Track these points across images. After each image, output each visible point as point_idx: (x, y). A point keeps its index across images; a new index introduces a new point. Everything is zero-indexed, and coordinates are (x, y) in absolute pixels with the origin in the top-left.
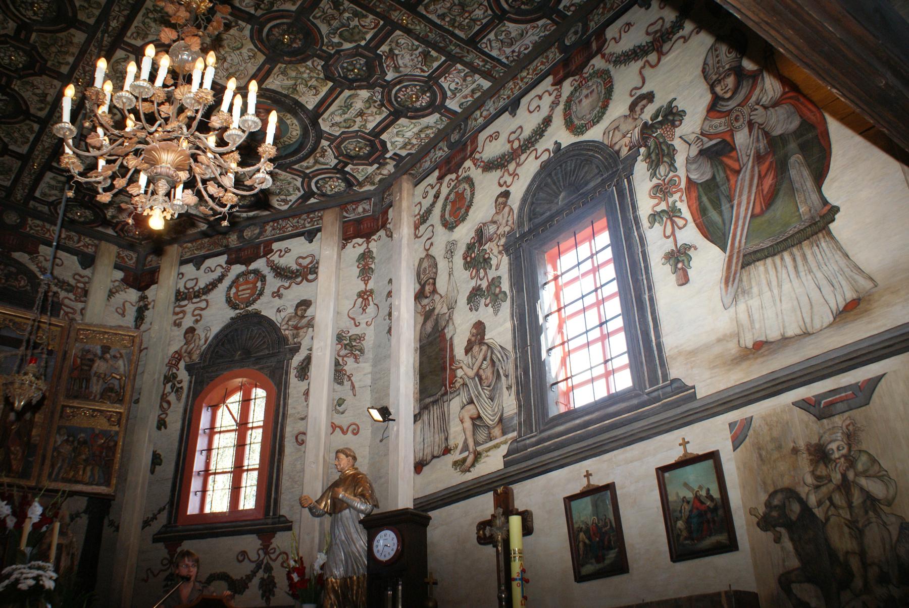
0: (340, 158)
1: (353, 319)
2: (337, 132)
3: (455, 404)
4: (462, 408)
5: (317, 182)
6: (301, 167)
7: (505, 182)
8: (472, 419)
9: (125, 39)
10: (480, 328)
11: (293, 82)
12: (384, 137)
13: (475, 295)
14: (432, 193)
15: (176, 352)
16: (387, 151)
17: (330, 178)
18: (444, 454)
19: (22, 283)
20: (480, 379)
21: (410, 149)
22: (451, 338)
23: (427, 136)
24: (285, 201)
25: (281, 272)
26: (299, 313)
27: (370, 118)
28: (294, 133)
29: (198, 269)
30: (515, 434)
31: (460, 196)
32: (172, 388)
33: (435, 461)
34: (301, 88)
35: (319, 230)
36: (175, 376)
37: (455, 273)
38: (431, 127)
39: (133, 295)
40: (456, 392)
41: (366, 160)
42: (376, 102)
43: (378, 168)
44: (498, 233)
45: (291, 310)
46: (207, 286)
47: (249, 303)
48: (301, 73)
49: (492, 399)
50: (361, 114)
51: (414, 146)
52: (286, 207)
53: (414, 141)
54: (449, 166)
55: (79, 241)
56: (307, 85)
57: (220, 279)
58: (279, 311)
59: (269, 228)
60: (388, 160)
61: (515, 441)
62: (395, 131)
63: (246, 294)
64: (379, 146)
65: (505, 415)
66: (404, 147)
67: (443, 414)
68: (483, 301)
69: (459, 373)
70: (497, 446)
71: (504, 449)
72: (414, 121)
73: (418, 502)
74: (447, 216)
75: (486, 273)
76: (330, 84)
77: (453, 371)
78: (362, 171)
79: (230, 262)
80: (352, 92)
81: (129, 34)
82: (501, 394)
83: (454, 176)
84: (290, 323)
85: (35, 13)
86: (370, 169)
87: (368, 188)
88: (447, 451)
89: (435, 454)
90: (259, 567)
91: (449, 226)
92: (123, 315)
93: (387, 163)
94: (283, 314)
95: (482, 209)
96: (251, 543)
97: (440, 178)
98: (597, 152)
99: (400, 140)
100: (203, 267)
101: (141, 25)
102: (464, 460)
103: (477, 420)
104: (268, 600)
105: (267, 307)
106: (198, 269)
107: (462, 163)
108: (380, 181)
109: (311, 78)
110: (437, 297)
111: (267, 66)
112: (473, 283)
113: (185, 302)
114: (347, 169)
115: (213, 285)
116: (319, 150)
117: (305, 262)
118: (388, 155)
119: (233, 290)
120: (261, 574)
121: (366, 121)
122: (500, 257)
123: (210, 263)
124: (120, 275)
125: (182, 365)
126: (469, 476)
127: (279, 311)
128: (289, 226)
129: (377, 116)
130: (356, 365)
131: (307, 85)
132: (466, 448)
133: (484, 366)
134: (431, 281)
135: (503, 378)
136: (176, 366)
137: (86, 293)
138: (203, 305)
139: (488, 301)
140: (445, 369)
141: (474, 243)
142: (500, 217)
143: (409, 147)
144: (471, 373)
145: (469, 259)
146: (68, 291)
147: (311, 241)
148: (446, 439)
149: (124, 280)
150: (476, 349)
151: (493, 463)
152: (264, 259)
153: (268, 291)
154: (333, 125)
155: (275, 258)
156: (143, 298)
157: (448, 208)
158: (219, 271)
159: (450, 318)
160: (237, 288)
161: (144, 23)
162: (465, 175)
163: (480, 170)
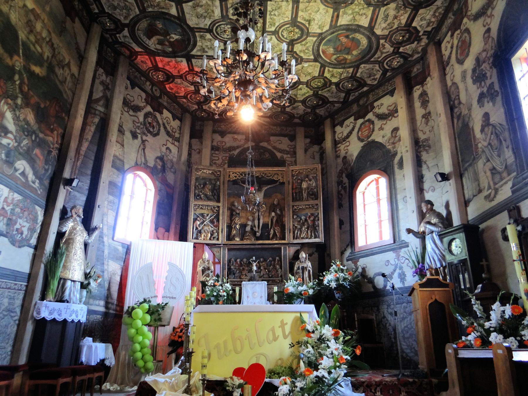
0: (394, 46)
1: (422, 131)
2: (386, 32)
3: (480, 164)
4: (484, 165)
5: (387, 64)
6: (375, 58)
7: (487, 23)
8: (491, 170)
9: (267, 30)
10: (486, 116)
11: (352, 16)
12: (414, 24)
13: (482, 96)
14: (449, 46)
15: (340, 170)
16: (419, 32)
17: (393, 59)
18: (479, 193)
19: (267, 156)
20: (491, 146)
21: (432, 25)
22: (473, 127)
23: (440, 13)
24: (375, 79)
25: (382, 117)
26: (394, 135)
27: (402, 17)
28: (364, 42)
29: (342, 127)
30: (515, 174)
31: (464, 42)
32: (342, 187)
33: (475, 198)
34: (357, 17)
35: (395, 89)
36: (342, 181)
37: (469, 89)
38: (441, 7)
39: (316, 148)
40: (480, 157)
41: (409, 41)
42: (401, 7)
43: (418, 43)
44: (488, 56)
45: (389, 135)
46: (348, 134)
47: (369, 137)
48: (354, 9)
49: (499, 156)
50: (395, 17)
51: (434, 22)
52: (376, 82)
53: (433, 20)
54: (456, 26)
55: (287, 130)
56: (359, 15)
57: (353, 129)
58: (383, 137)
59: (371, 96)
60: (422, 37)
61: (515, 178)
62: (419, 18)
63: (366, 133)
64: (412, 30)
65: (508, 164)
66: (428, 25)
67: (475, 170)
68: (486, 100)
69: (480, 145)
70: (506, 183)
71: (510, 184)
72: (428, 8)
73: (161, 230)
74: (459, 57)
75: (485, 83)
76: (372, 8)
77: (477, 145)
78: (407, 49)
79: (356, 119)
80: (385, 7)
81: (267, 26)
82: (504, 152)
83: (458, 32)
84: (390, 142)
85: (228, 35)
86: (414, 45)
87: (416, 56)
88: (480, 191)
89: (475, 194)
90: (396, 267)
91: (461, 62)
92: (314, 158)
93: (422, 39)
94: (386, 138)
95: (477, 45)
96: (390, 256)
97: (452, 36)
98: (215, 25)
99: (424, 23)
100: (344, 126)
101: (270, 20)
102: (490, 194)
103: (493, 170)
104: (403, 283)
105: (378, 137)
106: (342, 127)
107: (462, 21)
108: (422, 49)
109: (360, 10)
110: (461, 106)
111: (336, 14)
112: (479, 91)
113: (340, 145)
114: (401, 50)
115: (351, 133)
116: (381, 46)
117: (391, 108)
118: (421, 34)
119: (360, 133)
120: (398, 271)
121: (400, 20)
122: (491, 70)
123: (347, 122)
124: (308, 140)
125: (344, 175)
126: (493, 203)
127: (383, 137)
128: (380, 92)
129: (405, 15)
130: (428, 155)
131: (359, 15)
132: (489, 188)
133: (492, 138)
134: (457, 97)
135: (504, 142)
136: (341, 176)
137: (295, 153)
138: (348, 144)
139: (489, 99)
140: (471, 146)
141: (476, 67)
142: (487, 46)
143: (431, 24)
144: (486, 144)
145: (474, 78)
146: (287, 154)
147: (392, 96)
148: (479, 185)
149: (310, 142)
150: (486, 129)
151: (505, 193)
152: (371, 113)
153: (376, 128)
154: (383, 30)
155: (376, 110)
156: (321, 148)
157: (459, 51)
158: (351, 126)
159: (470, 115)
160: (361, 131)
161: (271, 19)
162: (464, 28)
163: (472, 22)
